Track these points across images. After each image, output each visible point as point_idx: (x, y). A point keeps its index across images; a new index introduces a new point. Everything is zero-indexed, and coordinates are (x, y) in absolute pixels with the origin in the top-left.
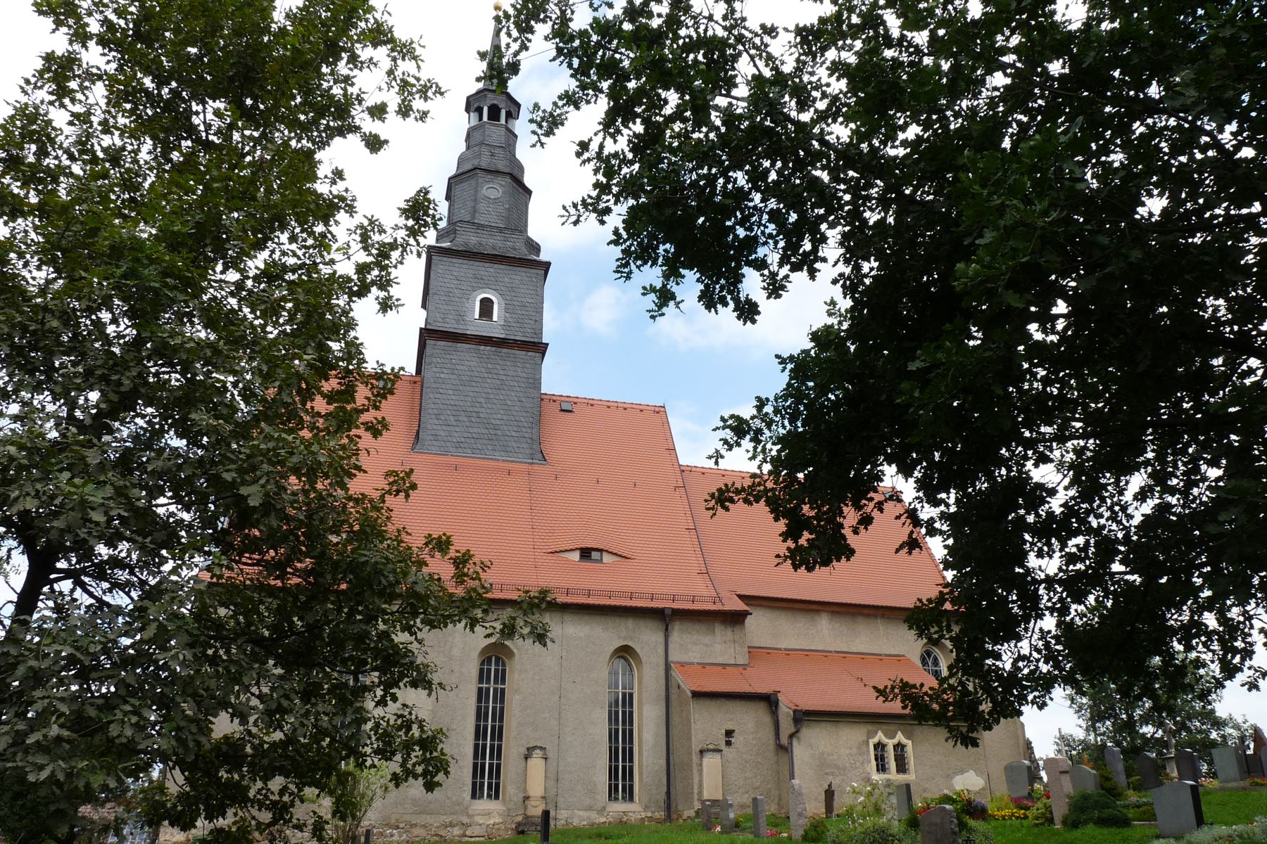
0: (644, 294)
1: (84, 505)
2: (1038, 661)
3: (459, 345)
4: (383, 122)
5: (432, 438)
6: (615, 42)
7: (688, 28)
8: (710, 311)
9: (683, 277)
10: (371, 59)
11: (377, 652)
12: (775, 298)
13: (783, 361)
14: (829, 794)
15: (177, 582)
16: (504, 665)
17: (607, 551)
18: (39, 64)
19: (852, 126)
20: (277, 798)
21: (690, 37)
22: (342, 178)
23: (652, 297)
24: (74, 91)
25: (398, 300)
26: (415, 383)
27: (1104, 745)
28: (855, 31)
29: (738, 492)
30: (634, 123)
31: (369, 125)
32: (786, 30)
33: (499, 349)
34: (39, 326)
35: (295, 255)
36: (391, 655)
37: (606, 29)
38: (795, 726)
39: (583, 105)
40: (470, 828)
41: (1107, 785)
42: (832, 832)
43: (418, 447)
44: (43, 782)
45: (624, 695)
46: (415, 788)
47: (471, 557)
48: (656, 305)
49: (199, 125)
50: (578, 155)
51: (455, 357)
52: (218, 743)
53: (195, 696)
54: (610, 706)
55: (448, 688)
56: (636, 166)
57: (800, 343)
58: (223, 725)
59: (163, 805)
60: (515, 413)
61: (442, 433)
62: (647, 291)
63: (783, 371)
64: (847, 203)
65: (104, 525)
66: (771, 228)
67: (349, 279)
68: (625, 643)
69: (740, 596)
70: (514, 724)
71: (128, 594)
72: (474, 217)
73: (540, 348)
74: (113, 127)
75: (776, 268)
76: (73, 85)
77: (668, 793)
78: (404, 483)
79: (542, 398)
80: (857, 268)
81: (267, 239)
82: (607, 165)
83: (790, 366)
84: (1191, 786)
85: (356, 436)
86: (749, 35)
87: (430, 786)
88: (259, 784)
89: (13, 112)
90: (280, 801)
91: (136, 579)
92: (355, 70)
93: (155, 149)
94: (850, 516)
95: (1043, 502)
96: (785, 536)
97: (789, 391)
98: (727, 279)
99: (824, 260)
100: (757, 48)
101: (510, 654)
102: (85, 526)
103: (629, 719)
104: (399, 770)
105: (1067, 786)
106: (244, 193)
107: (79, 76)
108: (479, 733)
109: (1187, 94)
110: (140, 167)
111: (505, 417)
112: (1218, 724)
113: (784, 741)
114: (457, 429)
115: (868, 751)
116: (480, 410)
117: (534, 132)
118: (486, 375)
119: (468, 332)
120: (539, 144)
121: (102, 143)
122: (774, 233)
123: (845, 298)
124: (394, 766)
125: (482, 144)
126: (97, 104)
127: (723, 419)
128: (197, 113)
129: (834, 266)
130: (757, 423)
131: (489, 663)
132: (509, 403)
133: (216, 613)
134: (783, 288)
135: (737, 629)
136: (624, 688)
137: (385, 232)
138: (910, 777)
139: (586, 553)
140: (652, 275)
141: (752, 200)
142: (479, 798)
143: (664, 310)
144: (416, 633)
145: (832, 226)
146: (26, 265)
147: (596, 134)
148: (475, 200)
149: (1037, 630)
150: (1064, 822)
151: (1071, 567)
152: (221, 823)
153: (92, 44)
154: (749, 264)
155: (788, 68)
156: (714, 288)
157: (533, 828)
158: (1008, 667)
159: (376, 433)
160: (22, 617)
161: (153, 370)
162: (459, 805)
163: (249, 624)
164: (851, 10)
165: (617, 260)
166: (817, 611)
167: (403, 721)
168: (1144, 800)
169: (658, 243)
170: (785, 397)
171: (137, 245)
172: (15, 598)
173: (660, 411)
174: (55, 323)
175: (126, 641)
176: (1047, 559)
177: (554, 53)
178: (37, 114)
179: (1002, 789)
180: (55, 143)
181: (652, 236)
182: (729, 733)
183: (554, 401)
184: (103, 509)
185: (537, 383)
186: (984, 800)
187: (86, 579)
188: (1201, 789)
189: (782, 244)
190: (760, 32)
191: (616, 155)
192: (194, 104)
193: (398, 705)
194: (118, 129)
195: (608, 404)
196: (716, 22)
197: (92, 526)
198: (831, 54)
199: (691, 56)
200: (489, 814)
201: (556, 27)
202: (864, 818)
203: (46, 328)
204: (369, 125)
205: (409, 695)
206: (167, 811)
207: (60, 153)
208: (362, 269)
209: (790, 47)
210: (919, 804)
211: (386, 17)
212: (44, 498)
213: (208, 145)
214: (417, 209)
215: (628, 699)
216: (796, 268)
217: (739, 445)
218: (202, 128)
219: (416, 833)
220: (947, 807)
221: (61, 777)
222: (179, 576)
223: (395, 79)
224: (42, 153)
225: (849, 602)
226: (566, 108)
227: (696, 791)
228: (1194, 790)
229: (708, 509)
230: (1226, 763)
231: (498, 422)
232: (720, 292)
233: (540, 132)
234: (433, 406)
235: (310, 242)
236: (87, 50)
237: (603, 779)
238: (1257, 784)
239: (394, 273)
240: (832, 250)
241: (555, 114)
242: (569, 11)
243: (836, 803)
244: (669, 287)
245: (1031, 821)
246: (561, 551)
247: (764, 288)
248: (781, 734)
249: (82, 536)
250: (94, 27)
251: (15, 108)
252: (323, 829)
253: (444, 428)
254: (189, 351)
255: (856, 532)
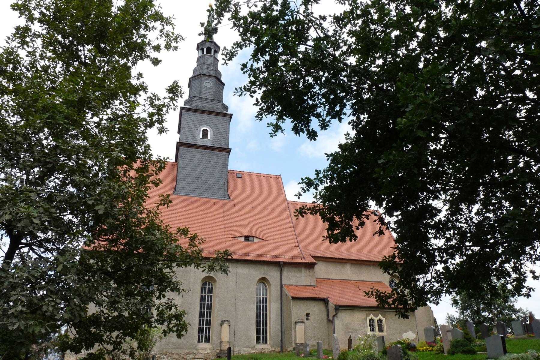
0: (268, 126)
1: (29, 216)
2: (434, 282)
3: (194, 149)
4: (159, 52)
5: (182, 188)
6: (258, 21)
7: (288, 16)
8: (297, 135)
9: (285, 120)
10: (154, 26)
11: (156, 277)
12: (324, 130)
13: (328, 156)
14: (350, 341)
15: (71, 248)
16: (212, 285)
17: (256, 237)
18: (14, 31)
19: (357, 56)
20: (115, 340)
21: (289, 19)
22: (142, 77)
23: (272, 128)
24: (28, 42)
25: (166, 128)
26: (175, 165)
27: (467, 321)
28: (358, 17)
29: (308, 209)
30: (266, 56)
31: (153, 54)
32: (330, 16)
33: (210, 151)
34: (14, 141)
35: (122, 110)
36: (161, 278)
37: (254, 16)
38: (336, 312)
39: (244, 48)
41: (467, 337)
42: (350, 356)
43: (176, 192)
44: (15, 330)
45: (263, 298)
46: (173, 337)
47: (197, 236)
48: (273, 131)
49: (81, 55)
50: (242, 69)
51: (192, 154)
52: (90, 316)
53: (79, 296)
54: (257, 303)
55: (187, 291)
56: (267, 73)
57: (336, 149)
58: (92, 309)
59: (67, 343)
60: (217, 178)
61: (186, 187)
62: (269, 125)
63: (328, 160)
64: (355, 90)
65: (39, 224)
66: (323, 100)
67: (146, 120)
68: (264, 276)
69: (312, 256)
70: (216, 310)
71: (52, 253)
72: (200, 95)
73: (228, 151)
74: (45, 57)
75: (325, 117)
76: (28, 39)
77: (282, 340)
78: (167, 200)
79: (229, 172)
80: (358, 118)
81: (110, 104)
82: (254, 72)
83: (331, 158)
84: (502, 337)
85: (148, 186)
86: (313, 19)
87: (179, 336)
88: (108, 334)
89: (3, 51)
90: (117, 341)
91: (55, 247)
92: (147, 32)
93: (63, 66)
94: (355, 222)
95: (436, 215)
96: (328, 230)
97: (330, 168)
98: (304, 122)
99: (345, 114)
100: (318, 25)
101: (215, 281)
102: (32, 225)
103: (265, 308)
104: (166, 329)
105: (450, 337)
106: (100, 85)
107: (31, 36)
108: (201, 314)
109: (491, 49)
110: (56, 74)
111: (213, 180)
112: (515, 311)
113: (331, 318)
114: (192, 185)
115: (367, 323)
116: (202, 177)
117: (223, 59)
118: (205, 162)
119: (197, 144)
120: (225, 64)
121: (40, 63)
122: (324, 103)
123: (353, 130)
124: (164, 327)
125: (204, 63)
126: (38, 48)
127: (302, 179)
128: (81, 50)
129: (348, 117)
130: (316, 181)
131: (206, 285)
132: (215, 174)
133: (89, 262)
134: (328, 125)
135: (311, 270)
136: (263, 295)
137: (160, 100)
138: (384, 334)
139: (247, 238)
140: (272, 119)
141: (315, 89)
142: (201, 342)
143: (277, 133)
144: (172, 269)
145: (348, 101)
146: (9, 115)
147: (250, 60)
148: (201, 88)
149: (434, 270)
150: (448, 352)
151: (449, 244)
152: (92, 351)
153: (36, 22)
154: (313, 115)
155: (330, 33)
156: (299, 125)
157: (224, 355)
158: (421, 285)
159: (157, 185)
160: (7, 261)
161: (62, 159)
162: (192, 345)
163: (103, 266)
164: (357, 8)
165: (258, 112)
166: (345, 263)
167: (168, 306)
168: (483, 343)
169: (275, 106)
170: (328, 171)
171: (54, 106)
172: (4, 255)
173: (279, 177)
174: (20, 139)
175: (50, 273)
176: (438, 240)
177: (232, 25)
178: (13, 52)
179: (423, 339)
180: (21, 64)
181: (272, 103)
182: (307, 315)
183: (234, 173)
184: (39, 218)
185: (226, 165)
186: (416, 344)
187: (34, 247)
188: (505, 339)
189: (327, 107)
190: (319, 18)
191: (258, 69)
192: (79, 47)
193: (166, 298)
194: (47, 58)
195: (257, 174)
196: (301, 14)
197: (35, 225)
198: (349, 27)
199: (290, 28)
200: (205, 349)
201: (233, 15)
202: (364, 350)
203: (16, 141)
204: (153, 54)
205: (169, 294)
206: (69, 345)
207: (23, 68)
208: (151, 115)
209: (332, 23)
210: (387, 345)
211: (160, 9)
212: (14, 214)
213: (85, 64)
214: (174, 90)
215: (265, 300)
216: (333, 117)
217: (308, 190)
218: (83, 56)
219: (174, 357)
220: (399, 345)
221: (22, 328)
222: (72, 244)
223: (163, 34)
224: (15, 68)
225: (359, 259)
226: (237, 49)
227: (293, 340)
228: (503, 338)
229: (295, 216)
230: (518, 328)
231: (210, 182)
232: (301, 127)
233: (226, 59)
234: (182, 175)
235: (128, 105)
236: (33, 24)
237: (254, 334)
238: (530, 337)
239: (165, 117)
240: (348, 110)
241: (232, 51)
242: (238, 8)
243: (352, 345)
244: (279, 124)
245: (435, 352)
246: (237, 237)
247: (320, 126)
248: (330, 315)
249: (31, 229)
250: (37, 14)
251: (4, 49)
252: (134, 354)
253: (187, 184)
254: (69, 150)
255: (358, 229)
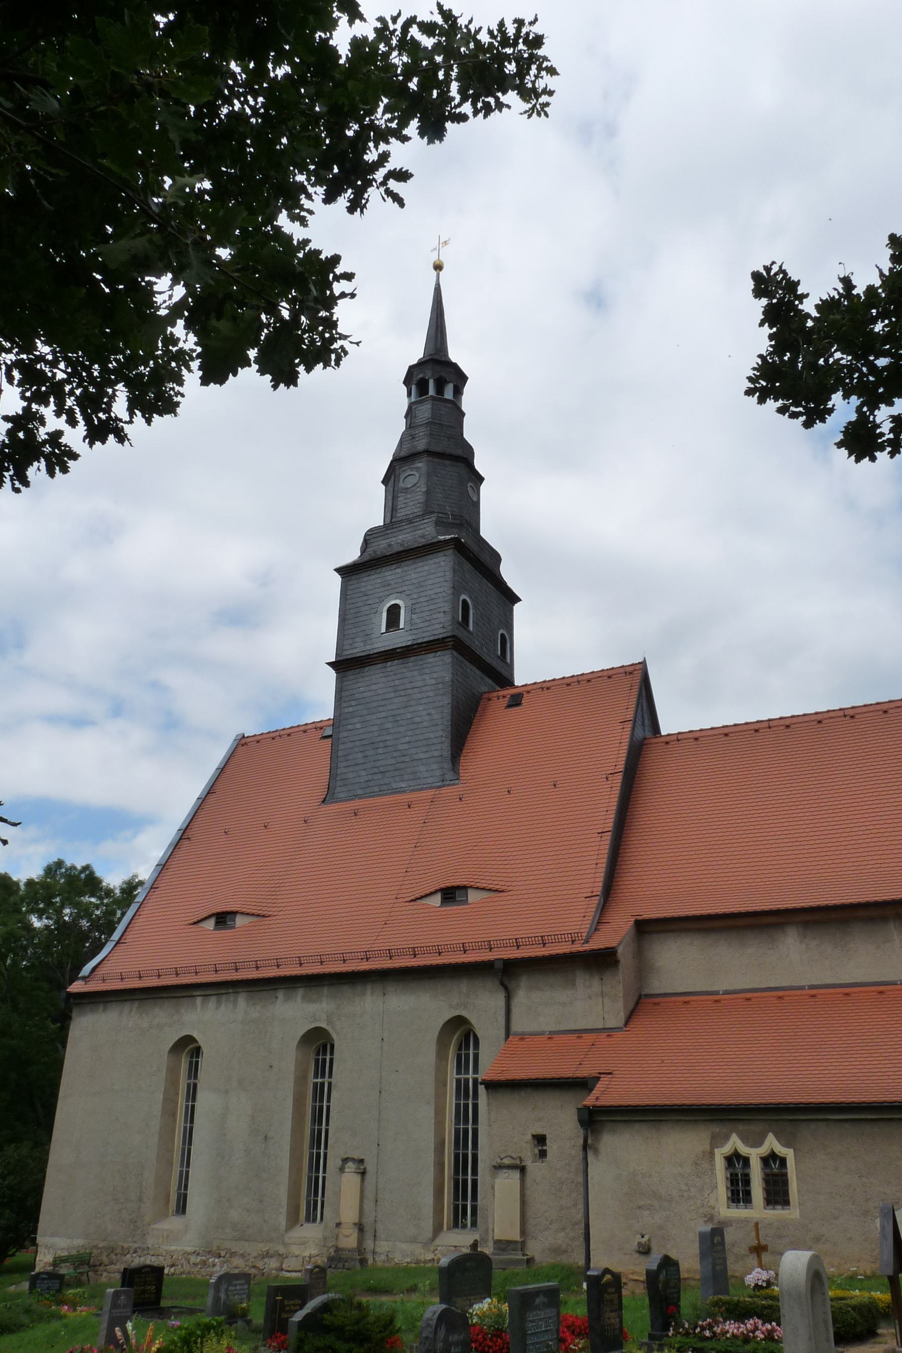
17: (471, 887)
40: (286, 1260)
68: (457, 1013)
115: (713, 1169)
219: (235, 1264)
231: (406, 746)
